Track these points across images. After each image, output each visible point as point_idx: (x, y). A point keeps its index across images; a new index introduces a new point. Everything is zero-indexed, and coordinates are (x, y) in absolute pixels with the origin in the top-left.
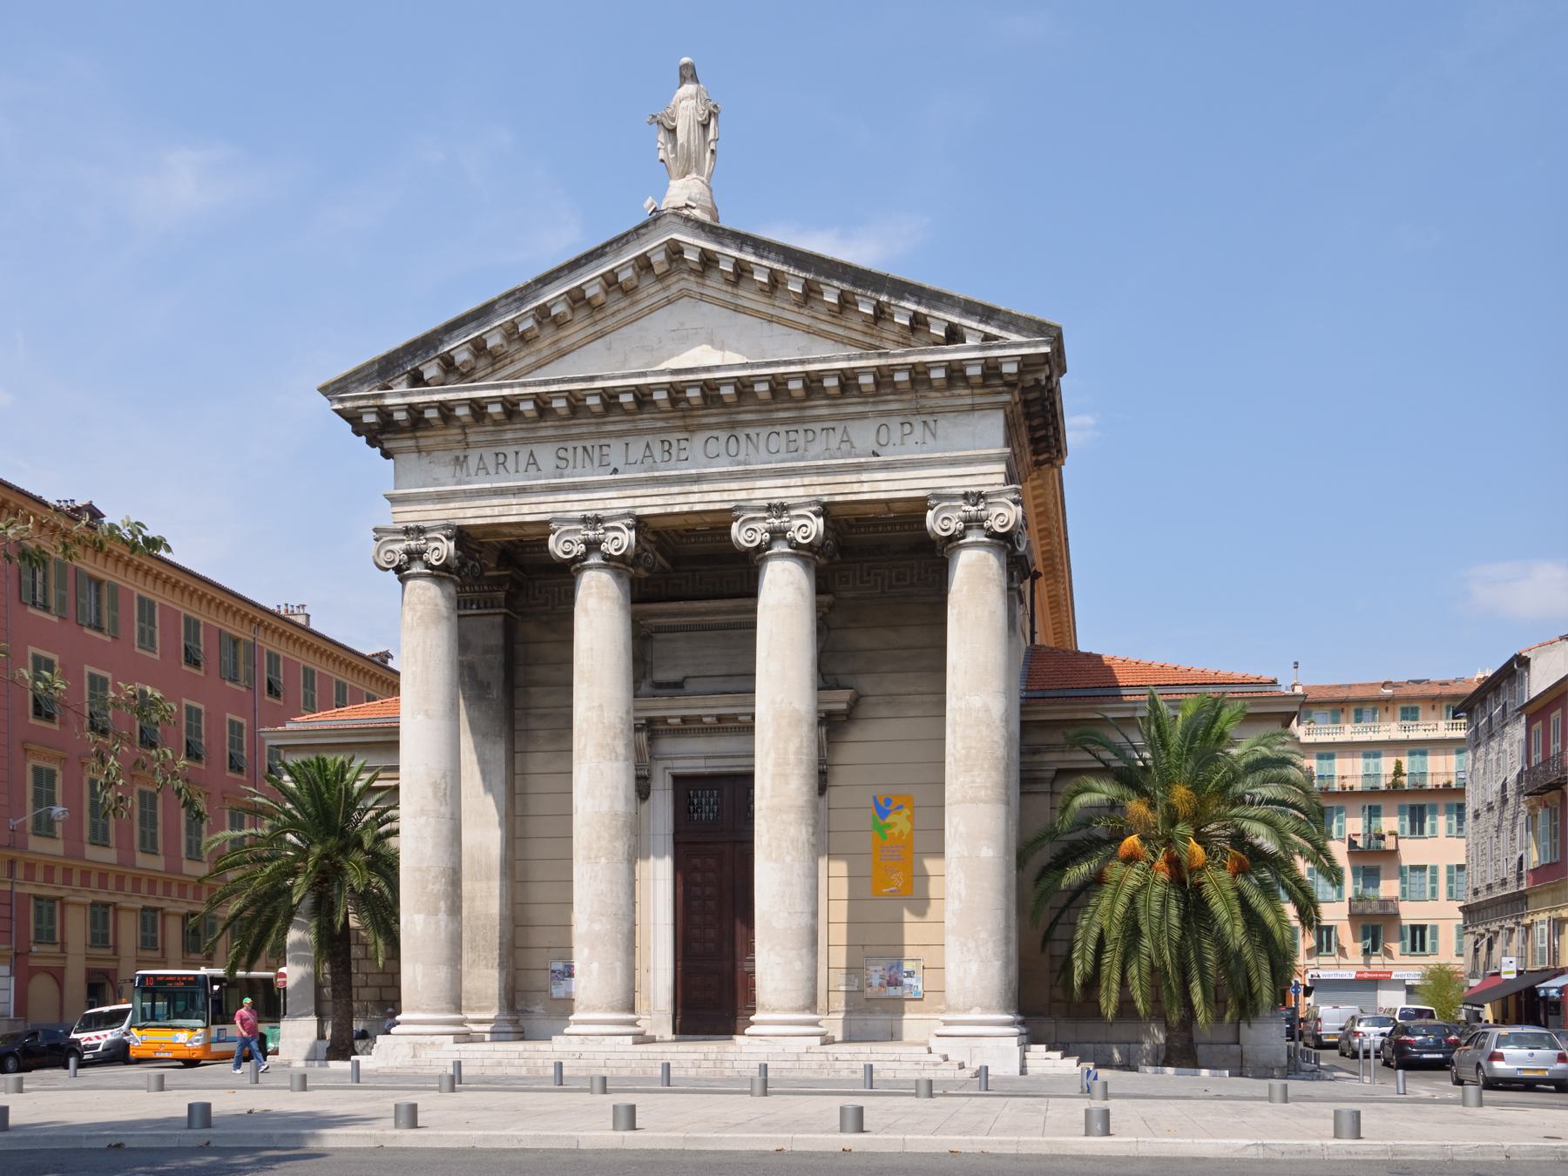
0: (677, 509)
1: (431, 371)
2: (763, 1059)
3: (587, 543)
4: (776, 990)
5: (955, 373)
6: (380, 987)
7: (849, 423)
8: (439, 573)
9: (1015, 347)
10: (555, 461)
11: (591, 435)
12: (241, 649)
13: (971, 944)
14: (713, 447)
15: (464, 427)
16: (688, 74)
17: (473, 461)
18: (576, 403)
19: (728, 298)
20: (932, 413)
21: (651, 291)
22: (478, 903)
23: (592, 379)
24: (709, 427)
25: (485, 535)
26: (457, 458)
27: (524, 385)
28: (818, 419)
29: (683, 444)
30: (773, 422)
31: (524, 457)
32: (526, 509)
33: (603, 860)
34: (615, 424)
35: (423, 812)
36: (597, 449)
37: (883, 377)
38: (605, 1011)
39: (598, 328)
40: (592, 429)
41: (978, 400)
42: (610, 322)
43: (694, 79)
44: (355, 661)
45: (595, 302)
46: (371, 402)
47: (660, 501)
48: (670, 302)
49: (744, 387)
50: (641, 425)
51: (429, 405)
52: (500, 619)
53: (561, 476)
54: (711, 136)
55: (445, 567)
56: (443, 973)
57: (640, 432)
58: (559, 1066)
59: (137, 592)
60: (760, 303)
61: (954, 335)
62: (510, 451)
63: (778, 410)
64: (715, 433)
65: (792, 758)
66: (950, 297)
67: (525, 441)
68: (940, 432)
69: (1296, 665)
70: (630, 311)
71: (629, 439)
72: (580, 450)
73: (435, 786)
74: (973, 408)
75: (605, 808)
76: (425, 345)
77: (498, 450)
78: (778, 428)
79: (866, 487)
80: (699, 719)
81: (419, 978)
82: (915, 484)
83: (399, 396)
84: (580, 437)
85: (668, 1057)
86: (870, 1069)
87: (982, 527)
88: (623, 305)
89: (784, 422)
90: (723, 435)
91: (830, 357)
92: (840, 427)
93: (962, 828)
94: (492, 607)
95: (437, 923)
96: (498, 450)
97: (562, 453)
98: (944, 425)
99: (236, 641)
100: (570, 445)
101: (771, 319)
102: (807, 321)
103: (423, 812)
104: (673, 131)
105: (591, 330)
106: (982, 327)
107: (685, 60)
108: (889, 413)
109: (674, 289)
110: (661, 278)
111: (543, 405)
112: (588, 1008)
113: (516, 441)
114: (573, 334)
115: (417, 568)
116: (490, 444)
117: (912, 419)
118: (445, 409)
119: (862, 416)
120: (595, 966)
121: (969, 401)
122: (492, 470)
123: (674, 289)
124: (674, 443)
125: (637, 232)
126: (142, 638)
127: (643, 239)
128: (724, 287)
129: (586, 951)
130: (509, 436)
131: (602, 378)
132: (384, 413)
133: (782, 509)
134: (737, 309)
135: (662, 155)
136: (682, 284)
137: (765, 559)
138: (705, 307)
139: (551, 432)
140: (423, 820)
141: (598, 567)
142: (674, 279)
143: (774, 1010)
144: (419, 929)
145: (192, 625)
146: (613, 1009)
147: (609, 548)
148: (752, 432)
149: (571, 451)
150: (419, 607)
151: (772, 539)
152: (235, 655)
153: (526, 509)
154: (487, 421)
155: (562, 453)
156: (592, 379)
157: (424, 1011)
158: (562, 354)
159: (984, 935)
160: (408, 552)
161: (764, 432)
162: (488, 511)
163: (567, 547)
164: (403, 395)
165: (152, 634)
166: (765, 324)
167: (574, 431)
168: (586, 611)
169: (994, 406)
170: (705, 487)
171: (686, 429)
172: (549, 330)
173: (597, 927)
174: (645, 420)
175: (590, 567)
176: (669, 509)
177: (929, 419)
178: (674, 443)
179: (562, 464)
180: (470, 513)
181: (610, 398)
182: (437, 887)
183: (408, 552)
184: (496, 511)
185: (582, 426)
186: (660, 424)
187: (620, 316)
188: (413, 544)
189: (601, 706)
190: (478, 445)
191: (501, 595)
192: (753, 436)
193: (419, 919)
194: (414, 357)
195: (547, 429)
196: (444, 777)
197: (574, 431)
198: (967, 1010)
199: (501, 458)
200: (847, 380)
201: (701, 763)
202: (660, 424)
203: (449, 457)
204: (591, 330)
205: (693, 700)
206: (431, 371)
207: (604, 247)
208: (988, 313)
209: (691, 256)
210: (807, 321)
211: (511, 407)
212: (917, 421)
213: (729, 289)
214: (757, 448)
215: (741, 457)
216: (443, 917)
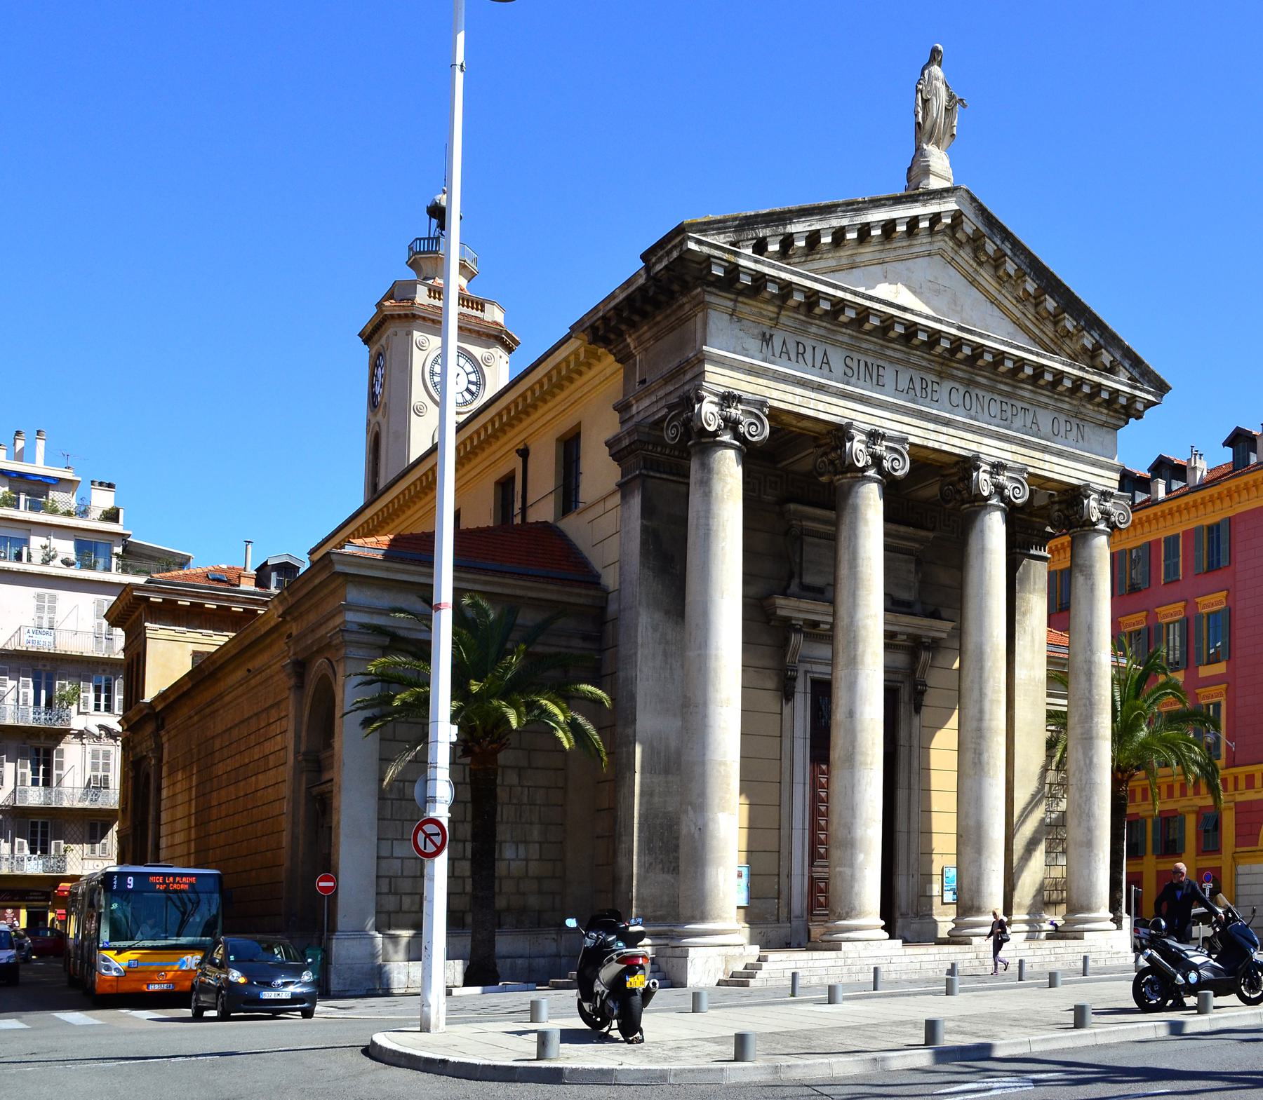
0: (931, 444)
2: (873, 963)
7: (1037, 409)
19: (971, 270)
20: (1082, 419)
22: (656, 799)
26: (764, 334)
28: (1022, 398)
29: (936, 387)
32: (821, 406)
36: (875, 368)
39: (883, 255)
41: (1109, 420)
42: (892, 254)
46: (726, 256)
51: (774, 280)
53: (848, 384)
57: (907, 363)
61: (1111, 370)
62: (809, 343)
63: (1001, 382)
66: (790, 211)
67: (823, 339)
69: (18, 433)
70: (905, 251)
71: (899, 368)
72: (862, 364)
77: (799, 339)
78: (996, 397)
79: (1047, 466)
82: (1073, 473)
84: (866, 352)
85: (953, 958)
88: (905, 244)
89: (1002, 393)
91: (999, 334)
92: (1032, 409)
94: (670, 473)
96: (799, 339)
100: (856, 356)
101: (993, 301)
107: (940, 47)
108: (1059, 410)
109: (937, 245)
116: (795, 331)
117: (1071, 420)
122: (793, 357)
123: (937, 245)
128: (971, 262)
130: (813, 329)
134: (973, 282)
138: (952, 271)
148: (981, 393)
153: (821, 406)
156: (905, 309)
158: (852, 267)
161: (988, 396)
162: (790, 398)
167: (864, 345)
170: (952, 431)
171: (940, 375)
176: (925, 443)
177: (1081, 423)
180: (775, 394)
184: (797, 400)
186: (924, 363)
187: (899, 252)
197: (864, 345)
202: (924, 363)
208: (1136, 362)
209: (968, 228)
212: (1074, 421)
213: (975, 265)
215: (973, 413)
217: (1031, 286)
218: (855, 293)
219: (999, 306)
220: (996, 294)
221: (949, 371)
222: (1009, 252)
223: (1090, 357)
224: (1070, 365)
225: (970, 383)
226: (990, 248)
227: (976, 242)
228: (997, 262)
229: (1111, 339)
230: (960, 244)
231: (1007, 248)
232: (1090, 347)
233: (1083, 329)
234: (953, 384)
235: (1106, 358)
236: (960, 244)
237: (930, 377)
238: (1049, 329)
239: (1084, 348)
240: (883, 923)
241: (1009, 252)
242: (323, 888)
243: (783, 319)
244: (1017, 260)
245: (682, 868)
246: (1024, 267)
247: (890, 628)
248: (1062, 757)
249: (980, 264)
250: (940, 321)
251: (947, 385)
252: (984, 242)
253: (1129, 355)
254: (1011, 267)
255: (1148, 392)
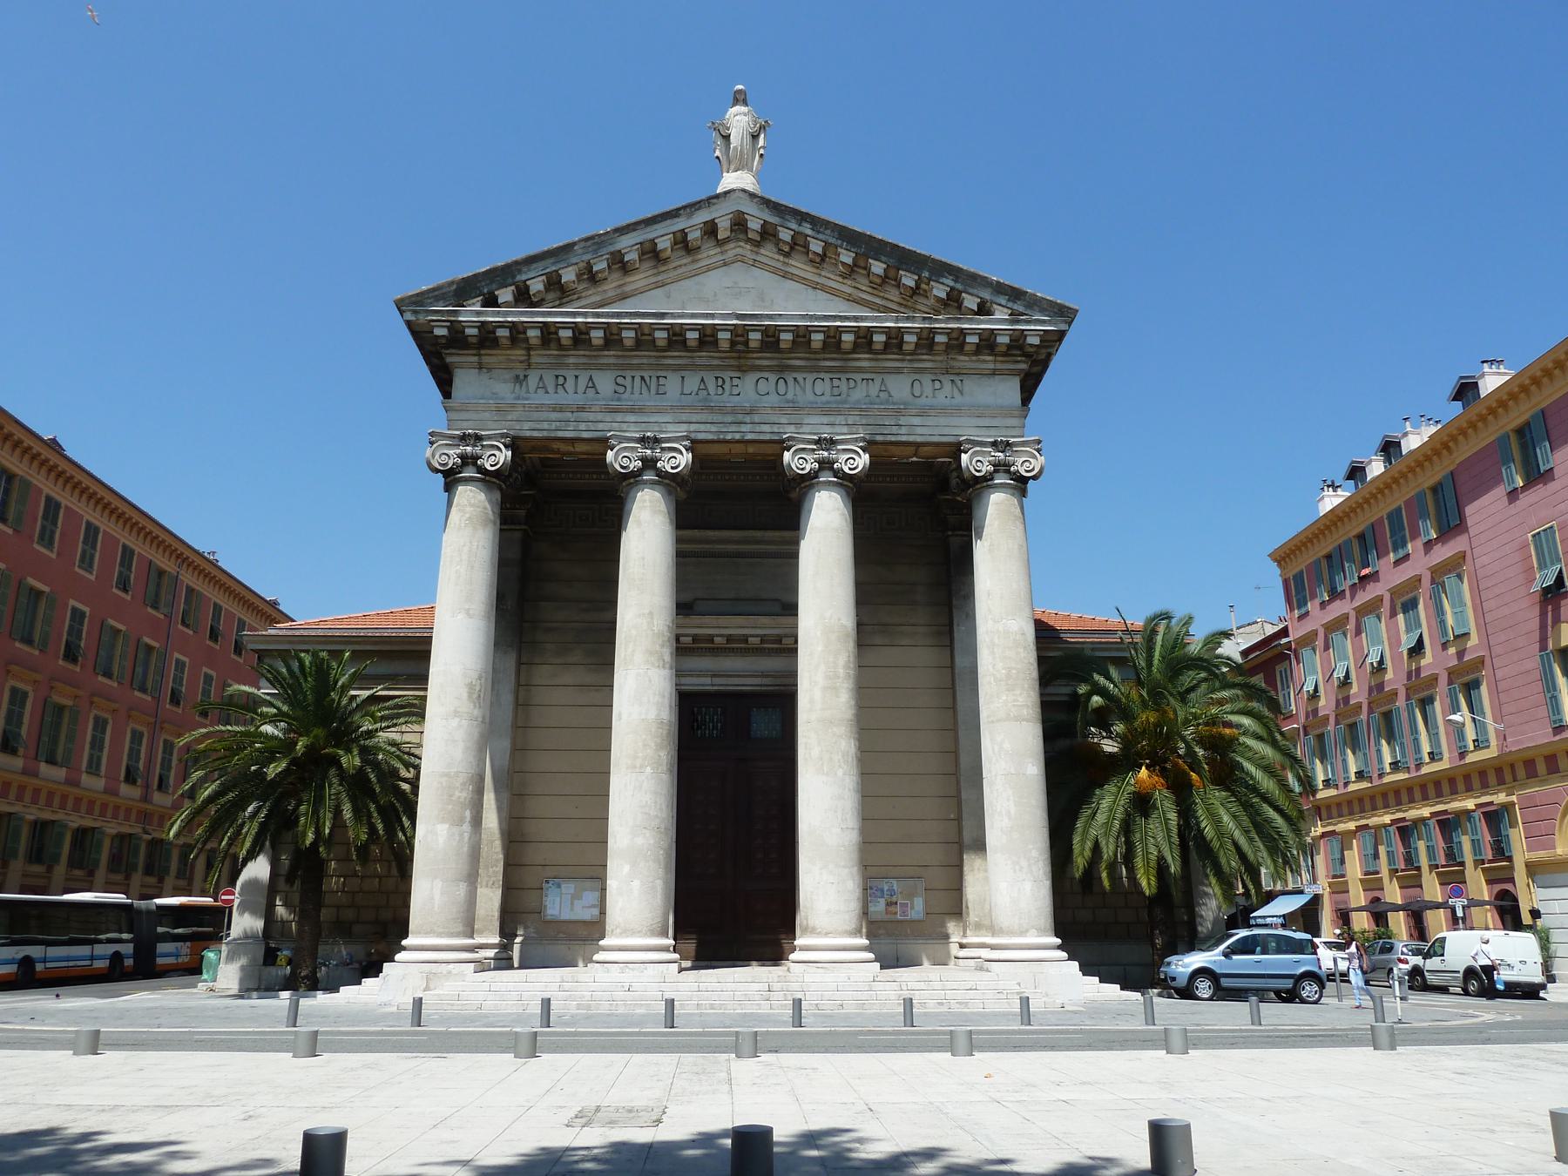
1: (505, 295)
3: (643, 459)
4: (828, 911)
5: (988, 342)
6: (338, 907)
7: (886, 377)
8: (489, 479)
9: (1036, 327)
10: (613, 387)
11: (651, 367)
12: (165, 580)
13: (1024, 863)
14: (762, 386)
15: (529, 349)
16: (739, 99)
17: (533, 380)
18: (644, 338)
19: (779, 265)
21: (710, 254)
23: (663, 316)
24: (760, 369)
25: (534, 449)
26: (517, 377)
27: (598, 315)
28: (860, 370)
29: (736, 382)
30: (817, 369)
31: (583, 381)
33: (649, 770)
34: (676, 357)
35: (456, 713)
37: (926, 340)
38: (645, 935)
40: (652, 361)
41: (999, 366)
42: (672, 274)
43: (745, 103)
44: (257, 602)
45: (663, 255)
47: (714, 428)
48: (725, 264)
49: (802, 336)
50: (698, 361)
52: (518, 535)
54: (761, 142)
55: (497, 474)
56: (462, 889)
57: (694, 368)
58: (546, 1003)
59: (87, 517)
60: (808, 272)
61: (983, 310)
62: (570, 375)
64: (766, 375)
65: (841, 671)
66: (516, 263)
67: (586, 367)
68: (966, 389)
71: (683, 373)
72: (638, 380)
73: (471, 686)
74: (994, 373)
75: (652, 715)
76: (503, 274)
78: (822, 375)
80: (710, 639)
81: (437, 897)
83: (472, 314)
84: (639, 367)
86: (909, 1003)
87: (1008, 472)
89: (829, 370)
90: (773, 377)
92: (878, 379)
93: (1007, 746)
95: (461, 835)
97: (620, 380)
98: (969, 384)
99: (161, 573)
100: (629, 374)
101: (815, 286)
102: (849, 290)
103: (456, 713)
104: (727, 138)
105: (653, 279)
106: (1010, 305)
107: (740, 87)
109: (731, 254)
110: (721, 243)
111: (612, 337)
112: (626, 932)
113: (577, 366)
114: (637, 280)
115: (469, 473)
116: (551, 366)
117: (941, 377)
118: (517, 330)
119: (898, 371)
120: (636, 884)
121: (992, 366)
122: (551, 389)
123: (731, 254)
124: (728, 380)
125: (695, 206)
126: (82, 559)
127: (713, 208)
129: (627, 868)
130: (571, 360)
131: (673, 316)
132: (456, 330)
133: (831, 443)
134: (786, 276)
135: (718, 153)
136: (739, 251)
137: (811, 486)
139: (612, 361)
140: (455, 722)
141: (653, 483)
142: (732, 245)
143: (827, 934)
144: (441, 840)
145: (128, 553)
146: (653, 933)
147: (666, 465)
148: (800, 377)
149: (629, 379)
150: (469, 509)
151: (820, 469)
152: (158, 585)
154: (553, 345)
155: (620, 380)
156: (663, 316)
157: (440, 935)
158: (624, 297)
159: (1035, 854)
160: (463, 457)
161: (810, 377)
163: (625, 462)
164: (478, 313)
165: (92, 557)
166: (810, 291)
167: (635, 361)
168: (639, 523)
169: (1012, 373)
171: (739, 368)
172: (616, 275)
173: (640, 841)
174: (703, 357)
175: (645, 482)
178: (728, 380)
179: (621, 390)
181: (677, 336)
182: (464, 794)
183: (463, 457)
185: (644, 357)
186: (716, 362)
187: (680, 271)
188: (469, 449)
189: (651, 613)
190: (540, 366)
191: (522, 513)
192: (800, 379)
193: (443, 830)
194: (492, 282)
195: (609, 357)
196: (480, 678)
197: (635, 361)
198: (1023, 933)
199: (561, 380)
200: (895, 339)
201: (708, 680)
202: (716, 362)
203: (508, 375)
204: (653, 279)
205: (707, 620)
206: (505, 295)
207: (679, 209)
208: (1015, 294)
209: (754, 225)
210: (849, 290)
211: (581, 335)
212: (946, 379)
214: (804, 390)
216: (467, 827)
217: (847, 257)
218: (723, 316)
219: (824, 288)
220: (817, 279)
221: (750, 362)
222: (809, 232)
223: (953, 302)
224: (908, 319)
225: (782, 369)
226: (785, 235)
227: (768, 233)
228: (798, 245)
229: (974, 279)
230: (757, 244)
231: (807, 229)
232: (943, 295)
233: (930, 280)
234: (759, 375)
235: (970, 302)
236: (757, 244)
237: (727, 375)
238: (893, 294)
239: (939, 299)
240: (1059, 941)
241: (809, 232)
242: (177, 835)
243: (534, 360)
244: (821, 236)
245: (1487, 962)
246: (831, 240)
247: (789, 620)
248: (1258, 766)
249: (787, 255)
250: (712, 316)
251: (750, 379)
252: (778, 232)
253: (1000, 288)
254: (816, 247)
255: (1043, 322)
